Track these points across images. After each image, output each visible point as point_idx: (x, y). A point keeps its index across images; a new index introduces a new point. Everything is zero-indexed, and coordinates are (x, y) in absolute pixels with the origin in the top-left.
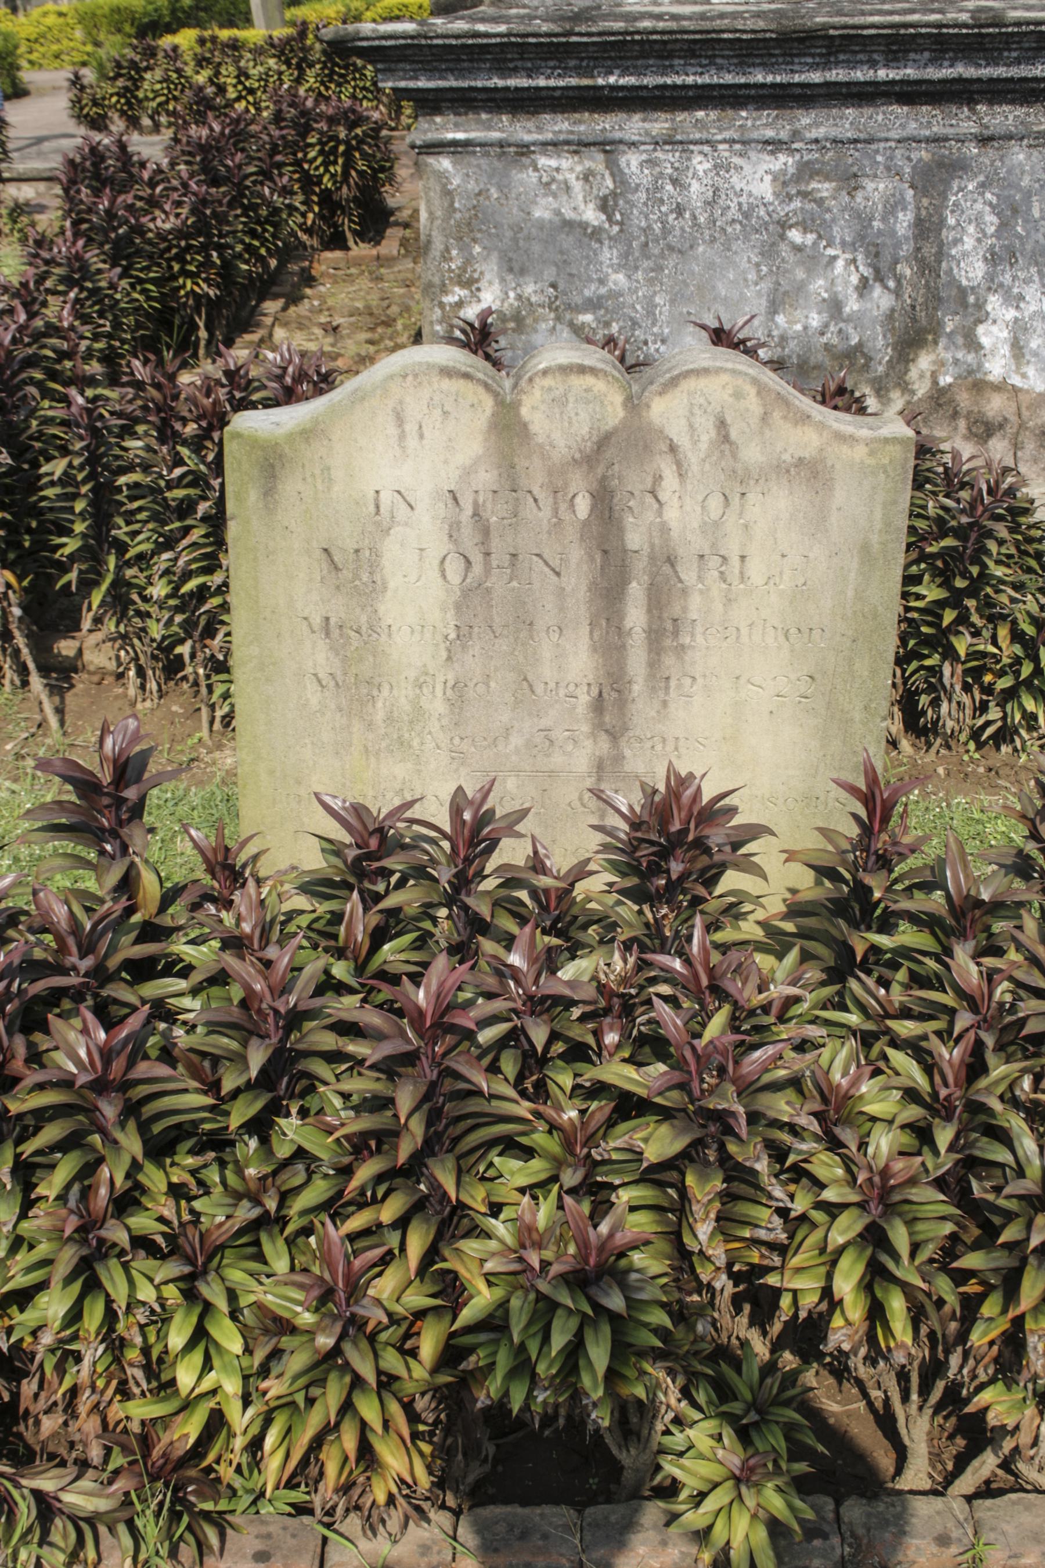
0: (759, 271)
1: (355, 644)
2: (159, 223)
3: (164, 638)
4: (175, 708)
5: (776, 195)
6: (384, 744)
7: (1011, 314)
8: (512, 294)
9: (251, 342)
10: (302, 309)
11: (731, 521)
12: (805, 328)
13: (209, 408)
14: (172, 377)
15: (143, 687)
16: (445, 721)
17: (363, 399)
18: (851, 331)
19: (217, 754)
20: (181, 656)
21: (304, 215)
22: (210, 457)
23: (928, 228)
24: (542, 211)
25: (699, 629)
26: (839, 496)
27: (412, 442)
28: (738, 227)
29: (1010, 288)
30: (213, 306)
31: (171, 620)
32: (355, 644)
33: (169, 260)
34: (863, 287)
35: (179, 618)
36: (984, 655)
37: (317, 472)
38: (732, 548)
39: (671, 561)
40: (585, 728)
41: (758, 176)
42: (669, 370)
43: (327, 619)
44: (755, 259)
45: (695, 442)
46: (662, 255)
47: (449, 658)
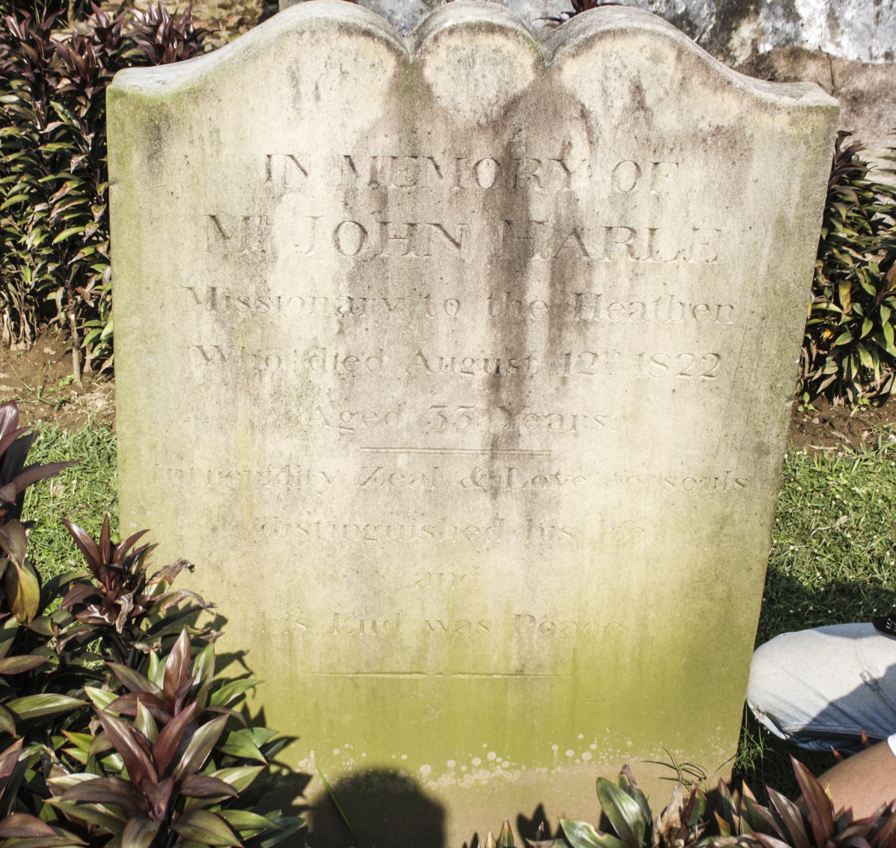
1: (242, 316)
3: (37, 285)
6: (270, 420)
13: (82, 64)
14: (46, 34)
15: (17, 330)
16: (335, 396)
17: (256, 56)
19: (88, 396)
20: (54, 301)
22: (83, 113)
25: (603, 305)
26: (757, 167)
27: (307, 103)
31: (44, 268)
32: (242, 316)
35: (51, 267)
36: (825, 313)
37: (206, 134)
38: (642, 221)
39: (577, 233)
40: (481, 405)
42: (583, 30)
43: (214, 289)
45: (608, 108)
47: (341, 332)
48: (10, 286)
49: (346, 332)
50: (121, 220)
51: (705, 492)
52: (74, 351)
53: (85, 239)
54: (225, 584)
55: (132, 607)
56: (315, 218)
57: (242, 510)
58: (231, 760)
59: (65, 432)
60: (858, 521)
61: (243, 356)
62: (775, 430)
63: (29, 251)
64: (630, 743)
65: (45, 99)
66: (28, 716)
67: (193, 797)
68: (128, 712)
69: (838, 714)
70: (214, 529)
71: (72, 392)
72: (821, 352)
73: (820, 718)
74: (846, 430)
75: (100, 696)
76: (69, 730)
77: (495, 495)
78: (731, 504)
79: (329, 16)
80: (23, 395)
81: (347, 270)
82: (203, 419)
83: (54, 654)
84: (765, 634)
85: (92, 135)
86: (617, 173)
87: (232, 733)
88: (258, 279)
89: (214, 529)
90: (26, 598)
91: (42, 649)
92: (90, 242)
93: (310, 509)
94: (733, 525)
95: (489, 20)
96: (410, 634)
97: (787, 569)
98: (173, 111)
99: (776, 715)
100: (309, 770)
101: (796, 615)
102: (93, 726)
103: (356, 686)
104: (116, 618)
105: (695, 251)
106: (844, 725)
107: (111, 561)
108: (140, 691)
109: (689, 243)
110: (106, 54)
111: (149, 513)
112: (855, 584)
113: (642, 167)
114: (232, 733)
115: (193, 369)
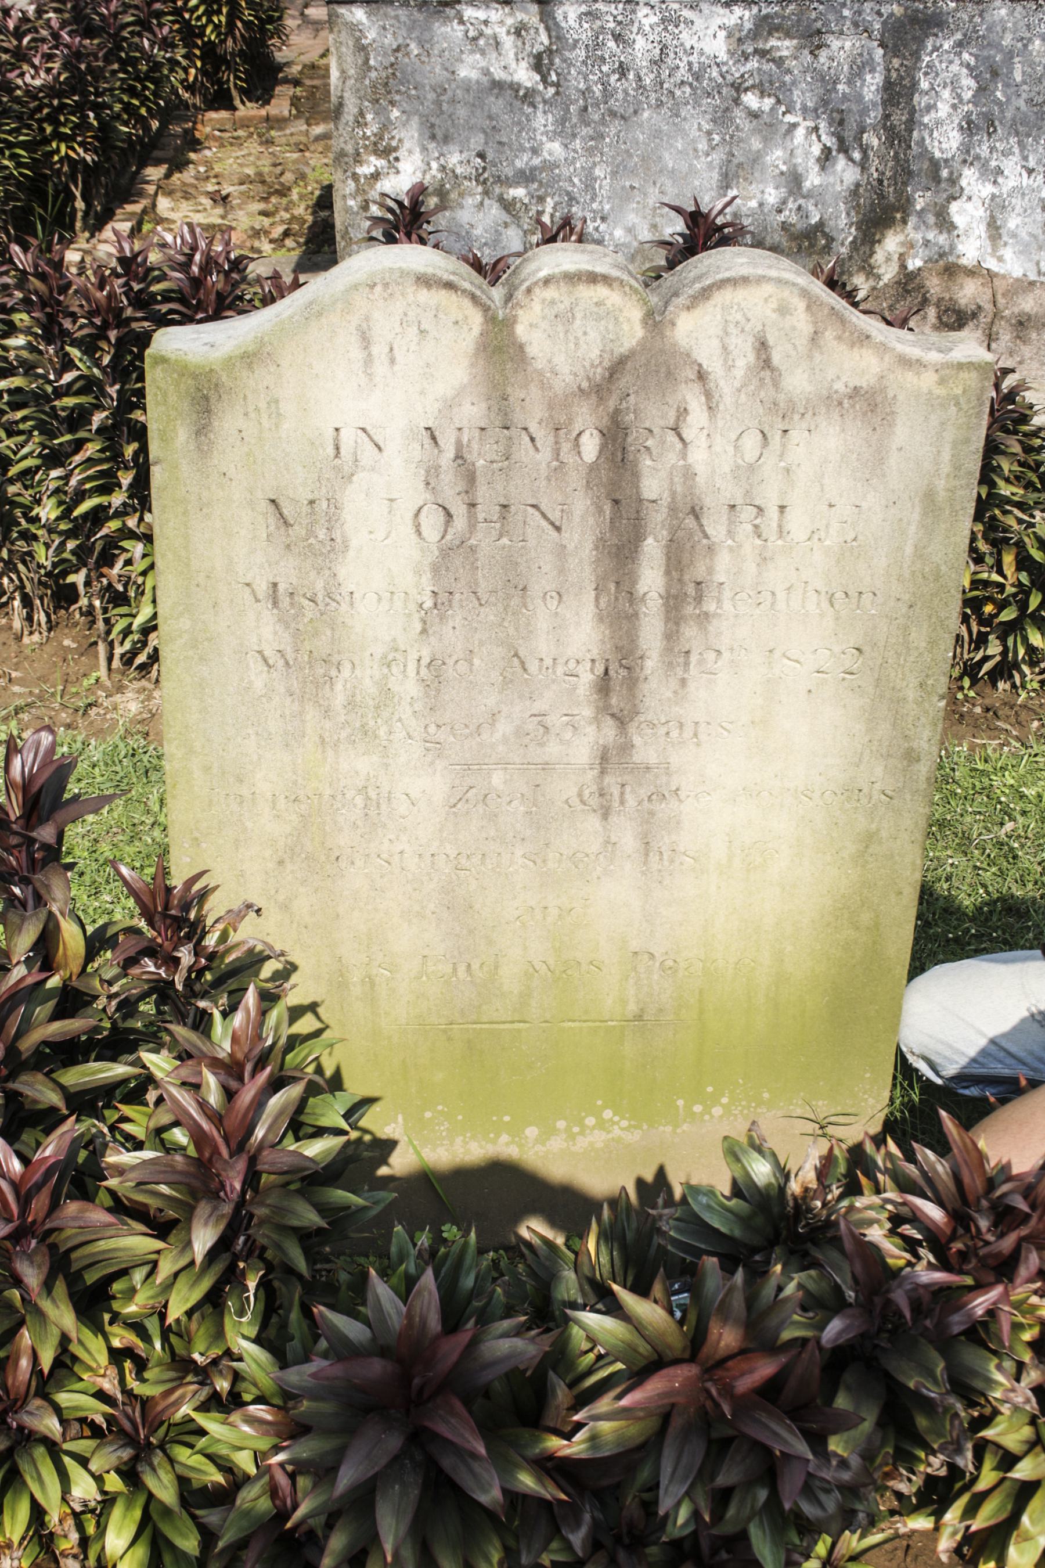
0: (710, 140)
1: (309, 615)
2: (28, 79)
3: (55, 565)
4: (67, 642)
5: (731, 53)
6: (344, 734)
7: (988, 189)
8: (434, 165)
9: (133, 214)
10: (188, 176)
11: (770, 463)
12: (761, 205)
13: (104, 301)
15: (29, 618)
17: (320, 314)
18: (811, 208)
19: (118, 698)
21: (186, 70)
22: (106, 360)
23: (898, 92)
24: (468, 70)
25: (727, 594)
26: (901, 433)
27: (380, 367)
28: (688, 90)
29: (987, 161)
30: (91, 173)
31: (63, 544)
32: (309, 615)
33: (40, 121)
34: (826, 158)
35: (71, 545)
36: (986, 584)
37: (263, 405)
38: (770, 497)
39: (695, 513)
40: (588, 712)
41: (711, 32)
42: (699, 278)
43: (275, 585)
44: (706, 127)
45: (730, 368)
46: (603, 122)
47: (424, 631)
48: (21, 567)
49: (430, 632)
50: (165, 507)
51: (848, 806)
52: (100, 643)
53: (111, 511)
54: (295, 925)
55: (193, 960)
56: (391, 500)
57: (312, 840)
58: (311, 1130)
59: (93, 742)
60: (1026, 828)
61: (311, 660)
62: (927, 733)
63: (44, 526)
64: (766, 1095)
65: (59, 344)
66: (78, 1089)
67: (270, 1173)
68: (193, 1080)
69: (1002, 1054)
70: (281, 862)
71: (100, 693)
72: (983, 629)
73: (981, 1059)
74: (1013, 720)
75: (159, 1062)
76: (120, 1102)
77: (605, 816)
78: (877, 819)
79: (404, 266)
80: (41, 698)
81: (430, 560)
82: (265, 735)
83: (104, 1016)
84: (919, 965)
85: (117, 387)
86: (740, 443)
87: (311, 1100)
88: (327, 572)
89: (281, 862)
90: (69, 953)
91: (89, 1011)
92: (118, 514)
93: (392, 837)
94: (880, 843)
95: (590, 268)
96: (510, 977)
97: (946, 886)
98: (224, 378)
99: (933, 1058)
100: (396, 1136)
101: (956, 940)
102: (151, 1096)
103: (449, 1039)
104: (175, 973)
105: (831, 531)
106: (1009, 1067)
107: (167, 907)
108: (204, 1056)
109: (824, 522)
110: (131, 289)
111: (204, 845)
112: (1023, 901)
113: (769, 435)
114: (311, 1100)
115: (253, 678)
